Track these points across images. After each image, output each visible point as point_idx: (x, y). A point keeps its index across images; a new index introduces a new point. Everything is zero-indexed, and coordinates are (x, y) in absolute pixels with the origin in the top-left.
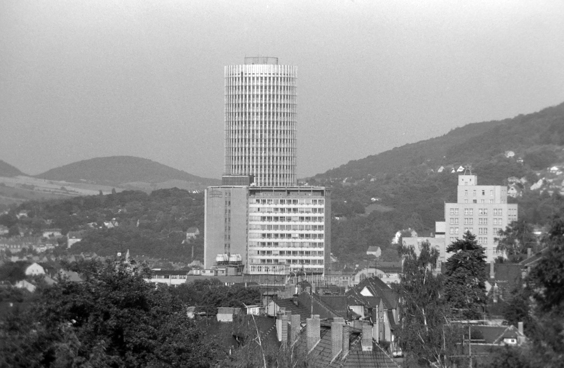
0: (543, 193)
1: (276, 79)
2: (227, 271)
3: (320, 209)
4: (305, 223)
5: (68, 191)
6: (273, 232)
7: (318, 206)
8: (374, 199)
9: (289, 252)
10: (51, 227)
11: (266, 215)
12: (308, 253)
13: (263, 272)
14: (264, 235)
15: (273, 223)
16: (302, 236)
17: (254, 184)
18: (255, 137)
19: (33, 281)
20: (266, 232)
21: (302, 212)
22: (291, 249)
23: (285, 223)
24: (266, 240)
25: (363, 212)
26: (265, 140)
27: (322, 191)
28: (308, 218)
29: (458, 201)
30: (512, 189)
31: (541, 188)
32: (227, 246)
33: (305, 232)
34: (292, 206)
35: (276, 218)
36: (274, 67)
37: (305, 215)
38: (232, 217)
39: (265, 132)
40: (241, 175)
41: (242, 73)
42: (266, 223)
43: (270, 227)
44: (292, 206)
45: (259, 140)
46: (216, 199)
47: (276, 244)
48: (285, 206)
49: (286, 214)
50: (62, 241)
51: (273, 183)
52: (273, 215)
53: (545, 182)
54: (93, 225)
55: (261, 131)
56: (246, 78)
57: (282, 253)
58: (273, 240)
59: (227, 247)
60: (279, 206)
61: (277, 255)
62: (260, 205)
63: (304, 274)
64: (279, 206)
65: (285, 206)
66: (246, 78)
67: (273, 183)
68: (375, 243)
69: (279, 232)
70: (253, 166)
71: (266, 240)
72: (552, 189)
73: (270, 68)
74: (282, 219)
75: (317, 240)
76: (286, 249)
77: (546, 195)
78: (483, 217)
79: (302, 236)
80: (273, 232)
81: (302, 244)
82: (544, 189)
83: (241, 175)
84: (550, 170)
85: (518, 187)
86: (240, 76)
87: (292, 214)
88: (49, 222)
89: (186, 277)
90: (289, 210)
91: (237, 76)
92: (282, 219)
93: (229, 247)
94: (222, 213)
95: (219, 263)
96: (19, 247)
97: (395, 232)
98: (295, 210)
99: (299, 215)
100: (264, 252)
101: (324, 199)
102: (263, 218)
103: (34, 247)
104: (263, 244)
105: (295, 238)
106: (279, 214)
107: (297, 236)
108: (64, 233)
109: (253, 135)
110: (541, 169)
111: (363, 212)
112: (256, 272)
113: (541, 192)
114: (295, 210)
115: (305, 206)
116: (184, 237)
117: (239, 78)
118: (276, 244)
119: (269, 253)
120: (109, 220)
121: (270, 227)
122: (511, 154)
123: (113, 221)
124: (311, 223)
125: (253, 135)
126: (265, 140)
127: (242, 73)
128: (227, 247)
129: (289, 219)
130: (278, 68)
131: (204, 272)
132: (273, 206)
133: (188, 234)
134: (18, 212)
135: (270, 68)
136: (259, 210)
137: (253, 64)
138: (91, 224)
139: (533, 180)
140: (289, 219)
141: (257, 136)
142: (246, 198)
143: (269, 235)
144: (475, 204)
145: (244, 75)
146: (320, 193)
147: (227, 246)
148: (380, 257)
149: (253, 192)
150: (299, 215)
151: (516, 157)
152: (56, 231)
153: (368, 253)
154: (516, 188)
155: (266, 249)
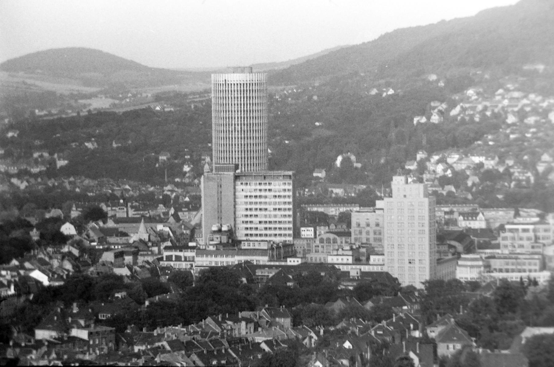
0: (460, 119)
1: (251, 84)
2: (221, 238)
3: (288, 190)
4: (277, 200)
5: (29, 85)
6: (253, 206)
7: (287, 187)
8: (317, 124)
9: (266, 222)
10: (40, 148)
11: (249, 194)
12: (280, 222)
13: (251, 247)
14: (247, 209)
15: (253, 200)
16: (275, 209)
17: (238, 171)
18: (236, 129)
19: (75, 245)
20: (249, 207)
21: (276, 191)
22: (268, 219)
23: (263, 200)
24: (249, 213)
25: (310, 135)
26: (244, 131)
27: (290, 176)
28: (280, 196)
29: (393, 195)
30: (435, 116)
31: (459, 115)
32: (220, 218)
33: (277, 207)
34: (268, 187)
35: (256, 197)
36: (250, 76)
37: (277, 194)
38: (222, 197)
39: (244, 125)
40: (229, 164)
41: (225, 80)
42: (249, 200)
43: (251, 203)
44: (268, 187)
45: (240, 132)
46: (211, 183)
47: (256, 216)
48: (263, 187)
49: (263, 193)
50: (52, 163)
51: (253, 170)
52: (254, 194)
53: (462, 107)
54: (75, 145)
55: (241, 125)
56: (228, 84)
57: (260, 222)
58: (254, 213)
59: (219, 219)
60: (259, 187)
61: (257, 224)
62: (244, 187)
63: (281, 247)
64: (259, 187)
65: (263, 187)
66: (228, 84)
67: (253, 170)
68: (320, 166)
69: (258, 206)
70: (235, 152)
71: (249, 213)
72: (469, 115)
73: (246, 76)
74: (260, 197)
75: (287, 213)
76: (263, 219)
77: (463, 121)
78: (411, 208)
79: (275, 209)
80: (253, 206)
81: (275, 216)
82: (462, 115)
83: (229, 164)
84: (466, 93)
85: (439, 113)
86: (224, 82)
87: (268, 193)
88: (37, 142)
89: (195, 251)
90: (266, 190)
91: (221, 83)
92: (260, 197)
93: (221, 218)
94: (214, 192)
95: (214, 232)
96: (16, 168)
97: (337, 156)
98: (270, 190)
99: (273, 193)
100: (247, 222)
101: (292, 182)
102: (246, 197)
103: (29, 168)
104: (247, 216)
105: (270, 211)
106: (258, 193)
107: (272, 209)
108: (51, 154)
109: (235, 128)
110: (458, 92)
111: (310, 135)
112: (246, 247)
113: (459, 118)
114: (270, 190)
115: (277, 187)
116: (157, 160)
117: (223, 84)
118: (256, 216)
119: (251, 222)
120: (89, 140)
121: (251, 203)
122: (433, 77)
123: (93, 141)
124: (282, 200)
125: (235, 128)
126: (244, 131)
127: (225, 80)
128: (219, 219)
129: (266, 197)
130: (252, 76)
131: (208, 247)
132: (253, 187)
133: (160, 158)
134: (7, 132)
135: (246, 76)
136: (243, 190)
137: (234, 73)
138: (73, 145)
139: (453, 105)
140: (266, 197)
141: (238, 128)
142: (233, 181)
143: (251, 209)
144: (405, 199)
145: (227, 82)
146: (289, 177)
147: (220, 218)
148: (325, 178)
149: (237, 177)
150: (273, 193)
151: (438, 81)
152: (44, 151)
153: (315, 175)
154: (438, 114)
155: (249, 219)
